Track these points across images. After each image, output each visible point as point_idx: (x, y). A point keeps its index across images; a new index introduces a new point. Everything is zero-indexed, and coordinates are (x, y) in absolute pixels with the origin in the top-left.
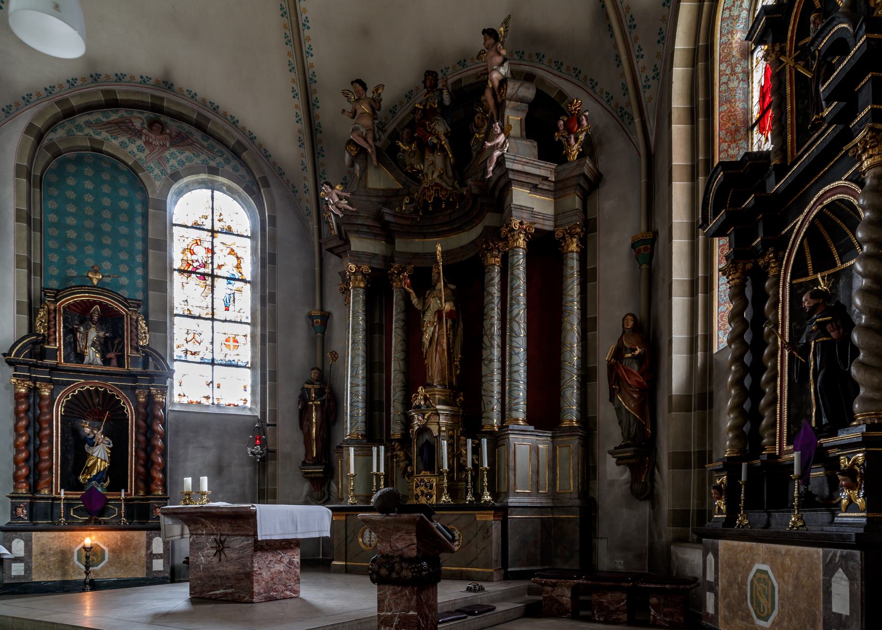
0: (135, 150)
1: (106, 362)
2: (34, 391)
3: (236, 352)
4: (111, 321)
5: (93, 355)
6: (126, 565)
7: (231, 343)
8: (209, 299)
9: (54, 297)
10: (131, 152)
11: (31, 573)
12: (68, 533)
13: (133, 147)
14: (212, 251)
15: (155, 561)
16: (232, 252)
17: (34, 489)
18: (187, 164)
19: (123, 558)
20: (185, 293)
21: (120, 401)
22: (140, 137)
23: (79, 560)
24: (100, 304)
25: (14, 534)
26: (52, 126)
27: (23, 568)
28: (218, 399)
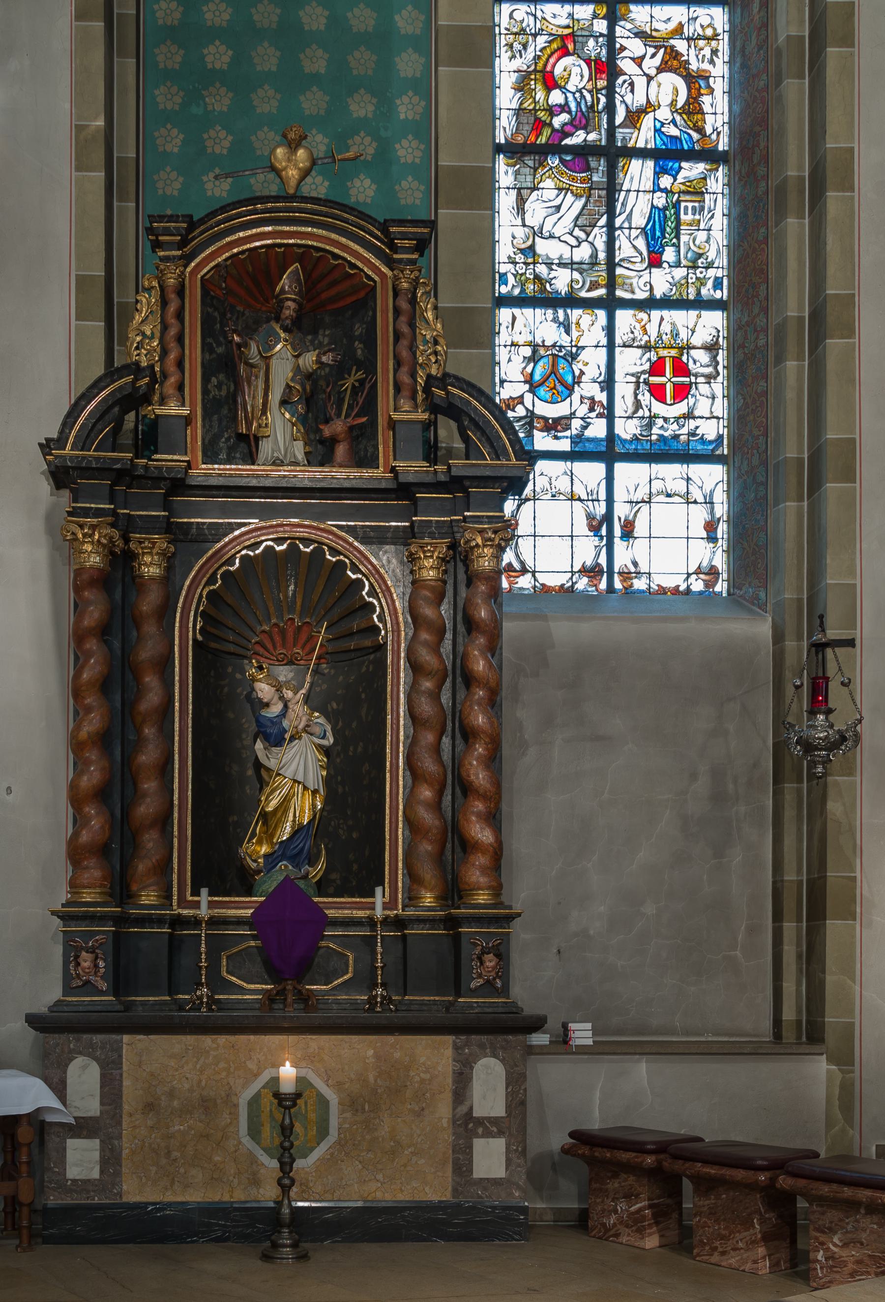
1: (321, 452)
2: (122, 561)
3: (681, 408)
4: (334, 306)
7: (668, 380)
8: (599, 238)
9: (181, 245)
11: (118, 1174)
12: (222, 1039)
14: (606, 68)
15: (479, 1144)
16: (673, 62)
17: (121, 889)
20: (534, 221)
21: (359, 584)
23: (254, 1132)
24: (304, 255)
25: (71, 1041)
27: (96, 1155)
28: (626, 576)
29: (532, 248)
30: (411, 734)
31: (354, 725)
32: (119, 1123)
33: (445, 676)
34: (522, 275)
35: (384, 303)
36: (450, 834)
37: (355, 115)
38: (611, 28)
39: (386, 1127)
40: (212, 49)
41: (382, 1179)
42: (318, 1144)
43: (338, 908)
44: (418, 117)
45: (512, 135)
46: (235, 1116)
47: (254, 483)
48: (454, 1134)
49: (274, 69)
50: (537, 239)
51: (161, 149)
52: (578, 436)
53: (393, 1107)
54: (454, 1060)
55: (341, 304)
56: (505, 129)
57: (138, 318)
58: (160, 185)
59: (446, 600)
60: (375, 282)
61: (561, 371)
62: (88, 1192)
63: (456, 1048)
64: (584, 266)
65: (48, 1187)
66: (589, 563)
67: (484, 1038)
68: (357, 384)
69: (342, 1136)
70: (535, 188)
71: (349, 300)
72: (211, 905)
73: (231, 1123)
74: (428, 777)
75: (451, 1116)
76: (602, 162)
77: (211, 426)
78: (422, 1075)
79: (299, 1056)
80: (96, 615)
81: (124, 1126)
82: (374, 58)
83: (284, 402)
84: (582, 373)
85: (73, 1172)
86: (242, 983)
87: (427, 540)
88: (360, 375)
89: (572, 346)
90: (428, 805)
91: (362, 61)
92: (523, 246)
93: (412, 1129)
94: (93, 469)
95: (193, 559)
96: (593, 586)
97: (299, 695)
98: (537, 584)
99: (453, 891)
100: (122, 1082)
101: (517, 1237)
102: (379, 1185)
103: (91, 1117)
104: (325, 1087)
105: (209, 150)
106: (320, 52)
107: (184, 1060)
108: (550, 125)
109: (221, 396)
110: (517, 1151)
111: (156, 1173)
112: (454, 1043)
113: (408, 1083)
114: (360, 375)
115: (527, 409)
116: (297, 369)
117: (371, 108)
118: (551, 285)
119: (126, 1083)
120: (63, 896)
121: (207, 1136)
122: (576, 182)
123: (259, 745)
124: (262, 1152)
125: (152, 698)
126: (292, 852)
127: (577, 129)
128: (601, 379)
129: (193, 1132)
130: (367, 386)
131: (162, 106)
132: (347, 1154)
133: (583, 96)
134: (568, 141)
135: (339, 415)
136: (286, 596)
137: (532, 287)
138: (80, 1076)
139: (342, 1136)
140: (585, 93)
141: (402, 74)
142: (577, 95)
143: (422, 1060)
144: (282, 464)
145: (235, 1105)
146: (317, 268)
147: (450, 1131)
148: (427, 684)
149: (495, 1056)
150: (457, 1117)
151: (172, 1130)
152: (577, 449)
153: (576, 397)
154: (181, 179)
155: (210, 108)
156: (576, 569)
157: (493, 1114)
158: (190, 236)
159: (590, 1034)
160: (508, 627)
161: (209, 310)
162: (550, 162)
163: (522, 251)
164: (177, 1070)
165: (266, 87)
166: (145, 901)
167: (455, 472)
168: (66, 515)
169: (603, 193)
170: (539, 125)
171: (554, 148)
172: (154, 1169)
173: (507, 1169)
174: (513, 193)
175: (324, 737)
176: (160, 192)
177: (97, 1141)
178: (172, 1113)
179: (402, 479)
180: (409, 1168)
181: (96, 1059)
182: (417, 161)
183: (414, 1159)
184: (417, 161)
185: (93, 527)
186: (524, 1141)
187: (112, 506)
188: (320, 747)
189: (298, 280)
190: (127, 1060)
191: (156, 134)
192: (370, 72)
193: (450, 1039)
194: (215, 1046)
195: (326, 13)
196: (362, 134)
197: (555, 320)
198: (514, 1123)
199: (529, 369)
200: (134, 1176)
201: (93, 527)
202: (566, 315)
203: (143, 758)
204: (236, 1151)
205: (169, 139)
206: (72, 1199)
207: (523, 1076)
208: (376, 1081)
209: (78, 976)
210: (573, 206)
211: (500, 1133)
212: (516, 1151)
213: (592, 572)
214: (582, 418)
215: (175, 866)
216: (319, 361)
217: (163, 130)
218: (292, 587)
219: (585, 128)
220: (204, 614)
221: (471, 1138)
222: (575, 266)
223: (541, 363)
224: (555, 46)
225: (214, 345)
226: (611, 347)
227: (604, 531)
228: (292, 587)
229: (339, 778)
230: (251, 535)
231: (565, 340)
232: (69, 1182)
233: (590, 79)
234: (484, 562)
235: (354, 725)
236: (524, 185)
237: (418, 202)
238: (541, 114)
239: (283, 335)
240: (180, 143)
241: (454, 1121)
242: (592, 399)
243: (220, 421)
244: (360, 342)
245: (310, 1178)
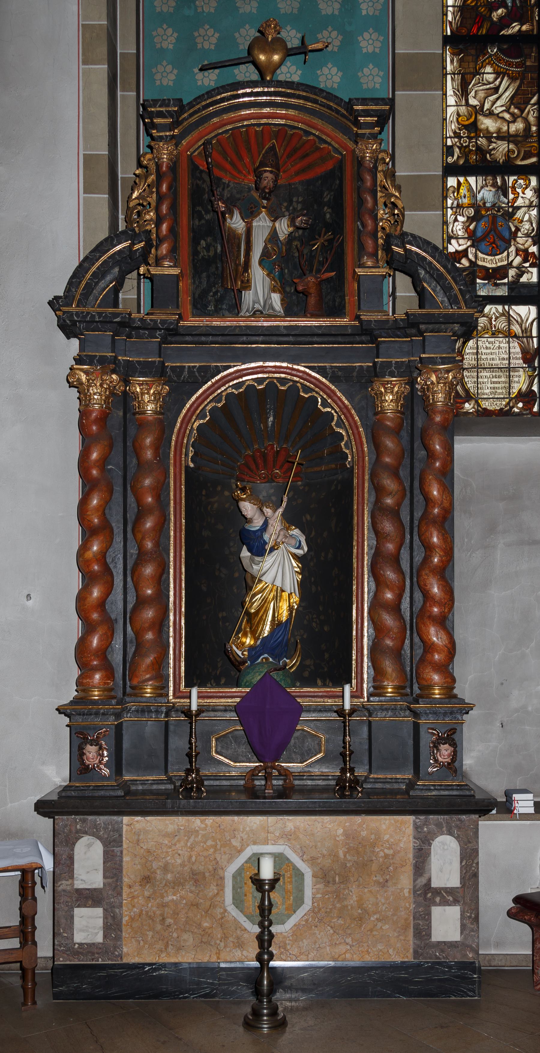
11: (118, 938)
15: (436, 911)
19: (352, 900)
23: (238, 902)
27: (100, 922)
30: (374, 546)
31: (325, 534)
32: (120, 894)
33: (404, 496)
34: (466, 147)
36: (408, 632)
37: (323, 13)
39: (354, 896)
41: (351, 943)
42: (295, 912)
45: (457, 28)
46: (221, 887)
48: (415, 902)
50: (480, 117)
51: (158, 46)
53: (361, 879)
54: (415, 838)
56: (450, 23)
58: (158, 77)
61: (499, 228)
62: (93, 954)
64: (519, 139)
65: (58, 950)
67: (441, 818)
68: (326, 244)
69: (316, 904)
73: (217, 894)
74: (389, 583)
75: (412, 887)
76: (534, 49)
77: (200, 283)
78: (386, 851)
79: (278, 835)
81: (124, 896)
84: (518, 230)
86: (230, 762)
89: (509, 207)
92: (467, 123)
93: (377, 898)
94: (97, 322)
95: (185, 398)
96: (527, 410)
97: (277, 513)
98: (479, 408)
100: (122, 857)
101: (470, 994)
102: (349, 947)
103: (95, 889)
104: (301, 862)
105: (199, 46)
107: (177, 838)
109: (209, 256)
111: (152, 937)
113: (374, 858)
115: (470, 261)
118: (490, 156)
119: (126, 859)
120: (71, 693)
122: (512, 67)
123: (245, 553)
124: (245, 919)
129: (184, 902)
130: (336, 244)
131: (158, 10)
132: (320, 921)
135: (311, 271)
137: (475, 157)
138: (85, 853)
139: (316, 904)
143: (386, 837)
145: (221, 878)
147: (412, 900)
149: (450, 833)
150: (417, 887)
152: (513, 294)
153: (512, 249)
154: (175, 72)
155: (199, 10)
157: (449, 885)
158: (180, 119)
161: (198, 182)
162: (489, 51)
163: (466, 127)
164: (170, 847)
168: (74, 363)
171: (494, 37)
173: (462, 933)
174: (458, 78)
175: (299, 548)
176: (158, 83)
178: (166, 885)
180: (374, 933)
181: (100, 838)
183: (379, 925)
187: (114, 354)
188: (295, 556)
190: (126, 838)
191: (154, 33)
194: (203, 826)
196: (330, 29)
197: (494, 185)
200: (133, 940)
202: (504, 181)
204: (222, 918)
205: (165, 37)
206: (79, 961)
208: (345, 856)
210: (507, 90)
211: (456, 902)
212: (470, 917)
214: (517, 268)
217: (160, 30)
218: (271, 419)
221: (429, 906)
222: (511, 139)
223: (482, 223)
225: (203, 212)
228: (271, 419)
229: (313, 579)
232: (77, 946)
235: (325, 534)
236: (467, 71)
240: (174, 41)
242: (526, 251)
243: (208, 277)
244: (329, 207)
245: (287, 942)
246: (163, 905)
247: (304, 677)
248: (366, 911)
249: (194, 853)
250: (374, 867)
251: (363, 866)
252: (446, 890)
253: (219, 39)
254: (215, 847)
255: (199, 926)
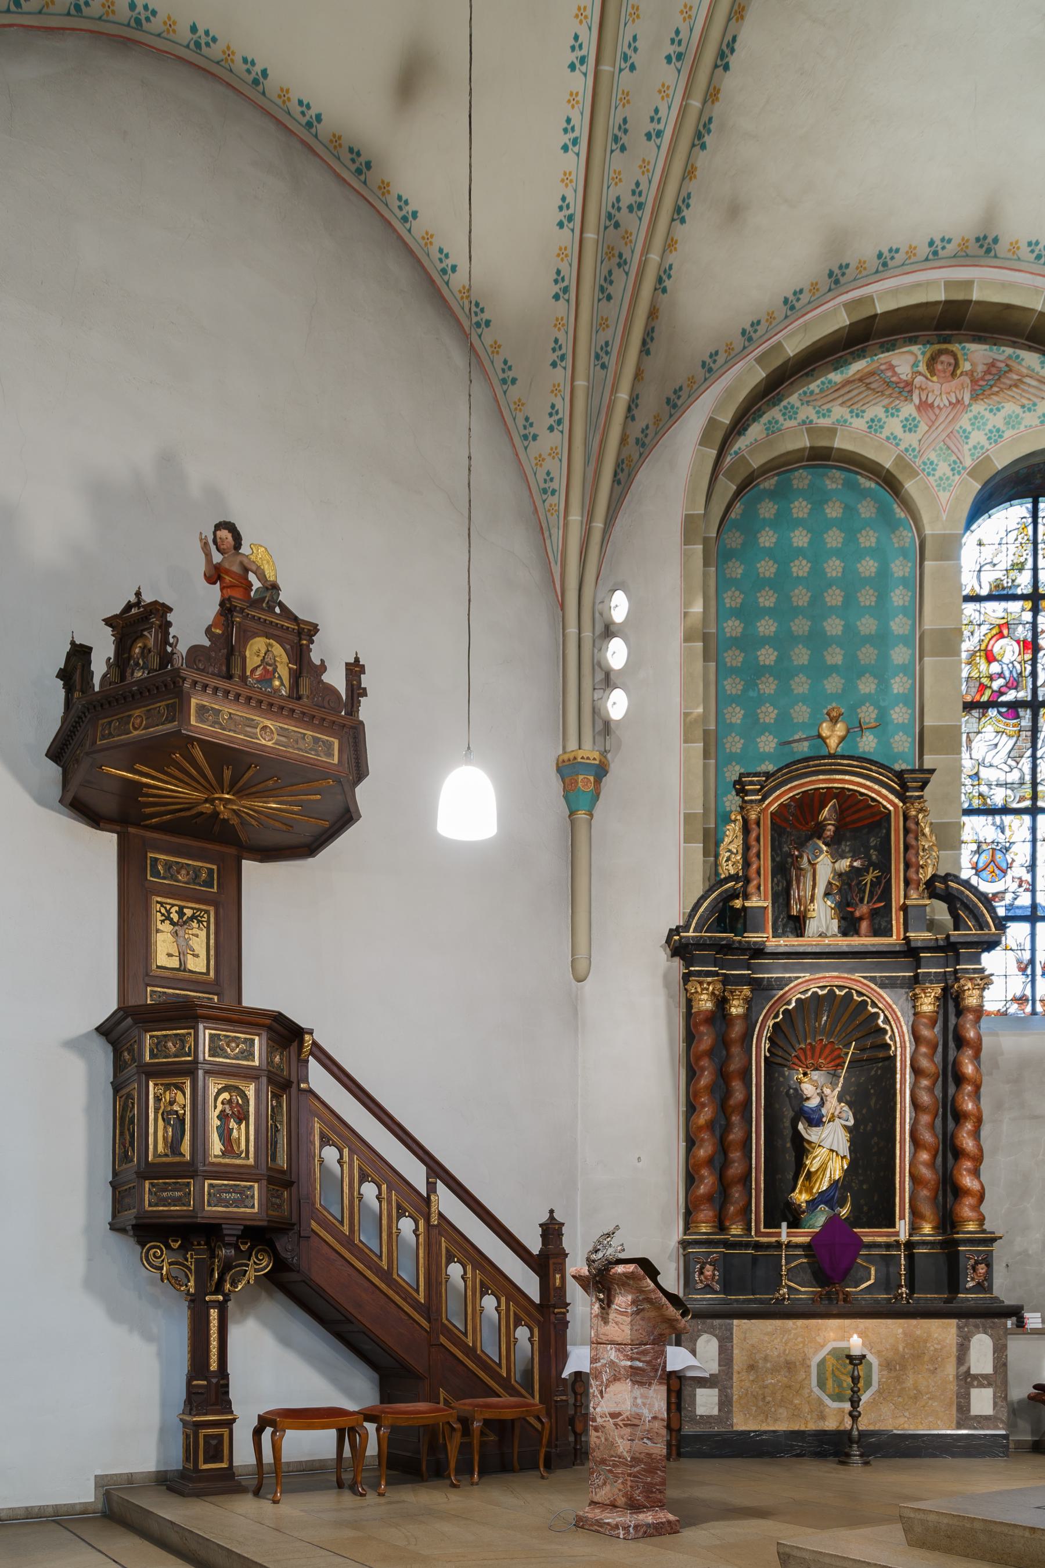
0: (899, 431)
1: (849, 926)
4: (864, 830)
5: (822, 918)
6: (916, 1398)
8: (1026, 765)
10: (893, 438)
11: (730, 1412)
12: (800, 1322)
13: (894, 426)
15: (974, 1392)
18: (1008, 434)
19: (909, 1383)
21: (876, 1016)
22: (908, 399)
23: (822, 1385)
24: (842, 795)
26: (739, 424)
27: (716, 1399)
29: (977, 774)
31: (864, 1111)
32: (732, 1379)
35: (897, 825)
38: (1035, 617)
40: (763, 651)
43: (869, 1235)
44: (906, 691)
46: (808, 1374)
47: (809, 950)
49: (806, 663)
50: (981, 768)
51: (728, 721)
52: (1011, 905)
55: (860, 824)
57: (727, 840)
58: (728, 746)
59: (938, 1025)
60: (890, 811)
63: (959, 1327)
66: (1018, 994)
67: (978, 1321)
70: (979, 732)
71: (866, 822)
72: (789, 1235)
80: (710, 1042)
82: (876, 652)
83: (827, 894)
84: (1013, 861)
85: (701, 1410)
87: (927, 985)
88: (877, 873)
90: (926, 1164)
91: (867, 655)
99: (948, 1222)
105: (762, 721)
106: (838, 650)
108: (990, 687)
110: (1001, 1396)
112: (958, 1325)
114: (877, 873)
116: (834, 870)
117: (873, 686)
119: (736, 1351)
121: (790, 1387)
125: (738, 1096)
126: (828, 1198)
127: (1010, 689)
128: (1027, 864)
131: (729, 692)
133: (1014, 667)
134: (1003, 699)
135: (862, 900)
136: (820, 1024)
140: (1016, 664)
141: (896, 662)
142: (1010, 666)
143: (936, 1335)
144: (826, 936)
146: (847, 800)
147: (955, 1383)
148: (925, 1082)
149: (985, 1333)
151: (766, 1382)
153: (1009, 877)
154: (742, 741)
156: (1009, 998)
159: (1040, 1320)
160: (985, 1040)
165: (801, 675)
166: (734, 1232)
167: (952, 939)
169: (1029, 734)
170: (982, 688)
172: (754, 1409)
177: (717, 1390)
179: (913, 944)
182: (906, 721)
184: (906, 721)
185: (709, 984)
186: (1006, 1390)
188: (845, 1127)
189: (836, 812)
191: (725, 711)
192: (873, 662)
193: (955, 1321)
195: (843, 623)
196: (867, 704)
197: (994, 824)
198: (999, 1378)
199: (975, 859)
201: (709, 984)
203: (731, 1137)
207: (1005, 1347)
209: (701, 1281)
210: (1006, 744)
211: (989, 1385)
213: (1021, 1000)
215: (753, 1208)
216: (851, 866)
218: (825, 1018)
219: (1016, 688)
220: (770, 1039)
224: (994, 632)
226: (1034, 841)
227: (1029, 971)
230: (804, 984)
231: (1001, 838)
233: (1020, 654)
234: (972, 1001)
235: (864, 1111)
237: (906, 750)
238: (984, 680)
239: (825, 848)
241: (957, 1376)
242: (1020, 878)
246: (765, 1387)
247: (858, 1219)
248: (920, 1392)
249: (787, 1348)
250: (926, 1358)
251: (918, 1357)
252: (982, 1375)
253: (777, 715)
254: (803, 1342)
255: (791, 1403)
